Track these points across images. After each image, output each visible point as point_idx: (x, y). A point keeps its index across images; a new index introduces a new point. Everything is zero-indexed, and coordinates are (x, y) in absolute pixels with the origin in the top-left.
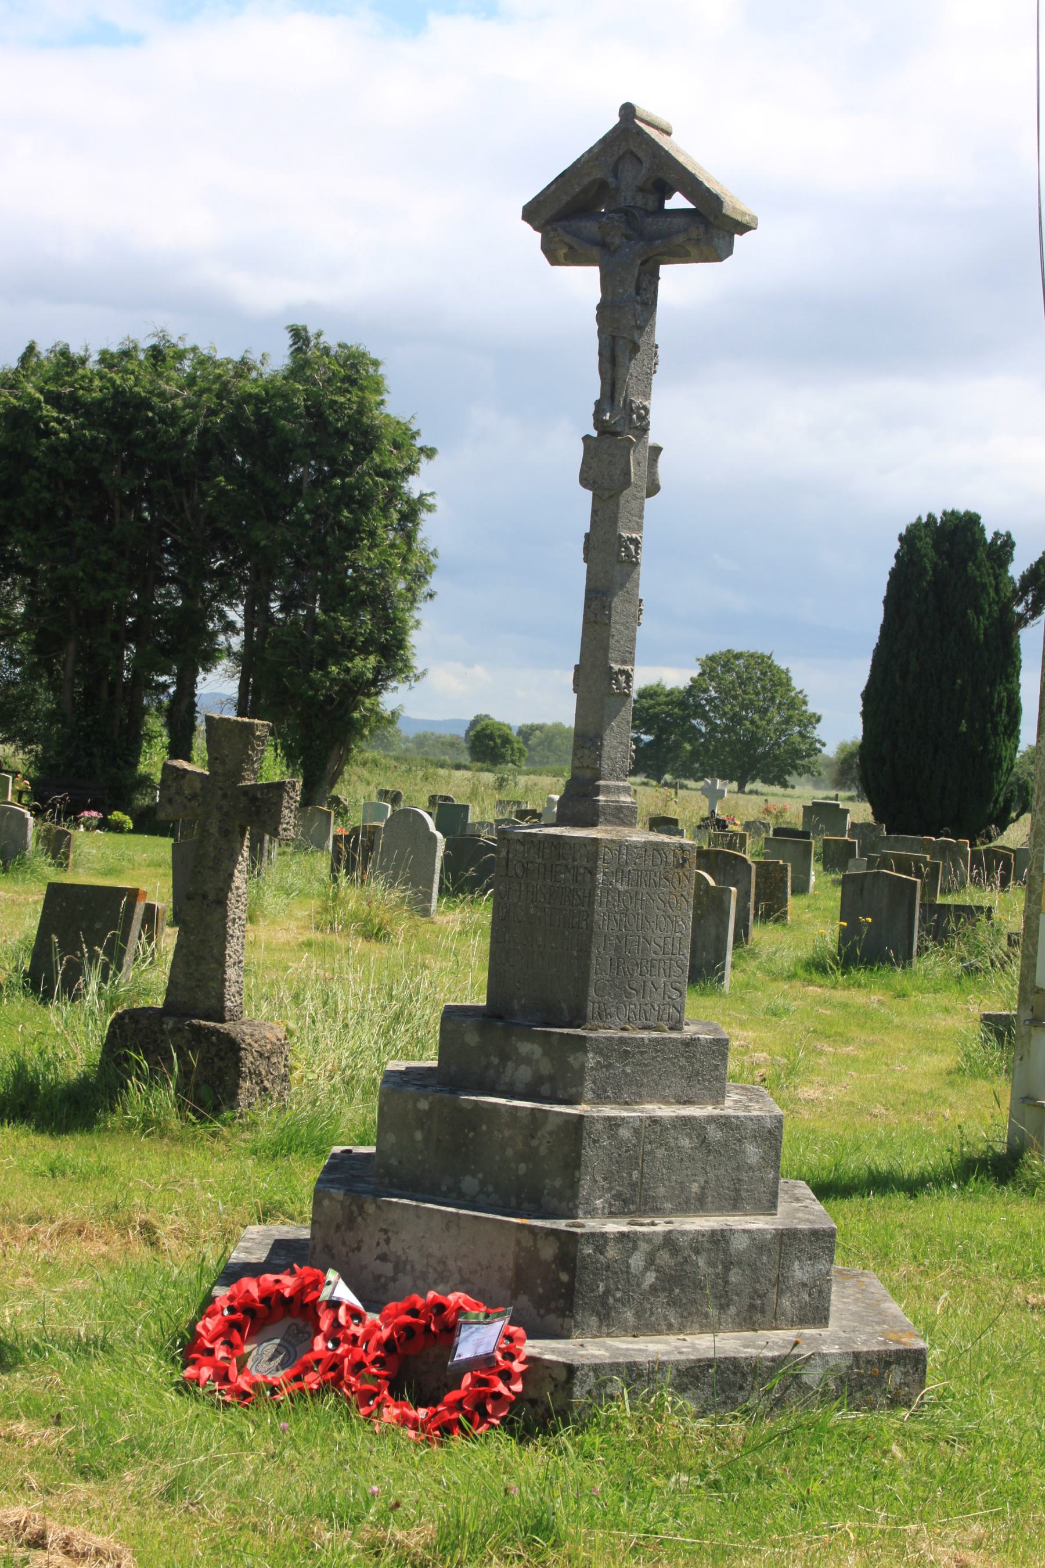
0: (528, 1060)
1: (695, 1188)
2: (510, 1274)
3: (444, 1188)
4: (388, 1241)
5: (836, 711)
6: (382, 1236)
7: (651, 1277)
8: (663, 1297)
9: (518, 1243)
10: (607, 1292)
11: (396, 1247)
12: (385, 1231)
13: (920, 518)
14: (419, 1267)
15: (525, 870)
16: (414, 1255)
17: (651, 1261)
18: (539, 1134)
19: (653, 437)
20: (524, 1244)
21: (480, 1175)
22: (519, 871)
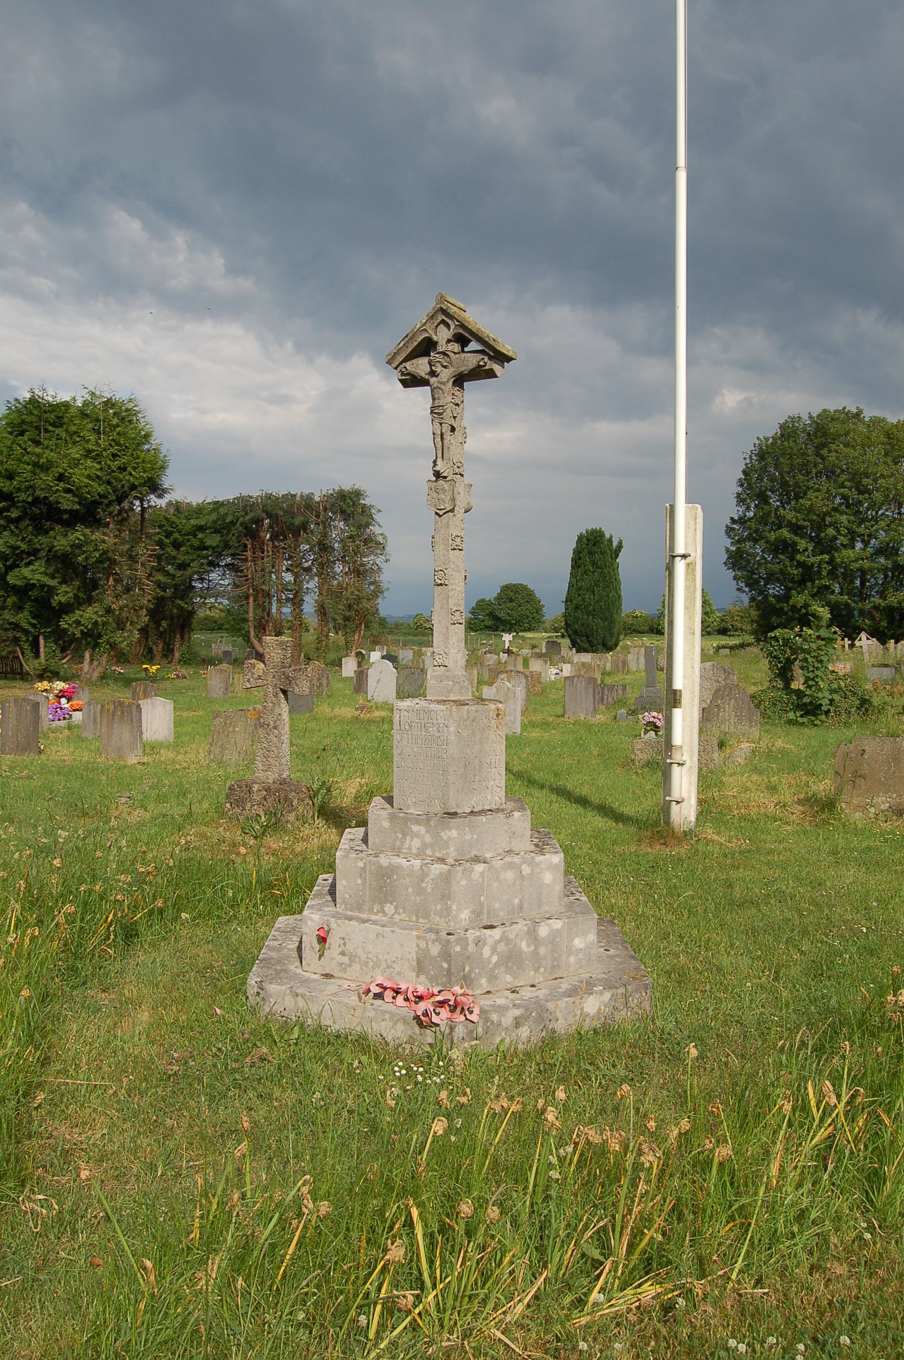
0: (417, 835)
1: (516, 901)
2: (415, 963)
3: (375, 911)
4: (345, 944)
5: (554, 606)
6: (342, 942)
7: (495, 959)
8: (503, 969)
9: (418, 946)
10: (470, 971)
11: (350, 947)
12: (343, 939)
13: (727, 550)
14: (363, 959)
15: (410, 726)
16: (360, 952)
17: (494, 950)
18: (426, 880)
19: (607, 536)
20: (421, 945)
21: (395, 903)
22: (407, 727)
